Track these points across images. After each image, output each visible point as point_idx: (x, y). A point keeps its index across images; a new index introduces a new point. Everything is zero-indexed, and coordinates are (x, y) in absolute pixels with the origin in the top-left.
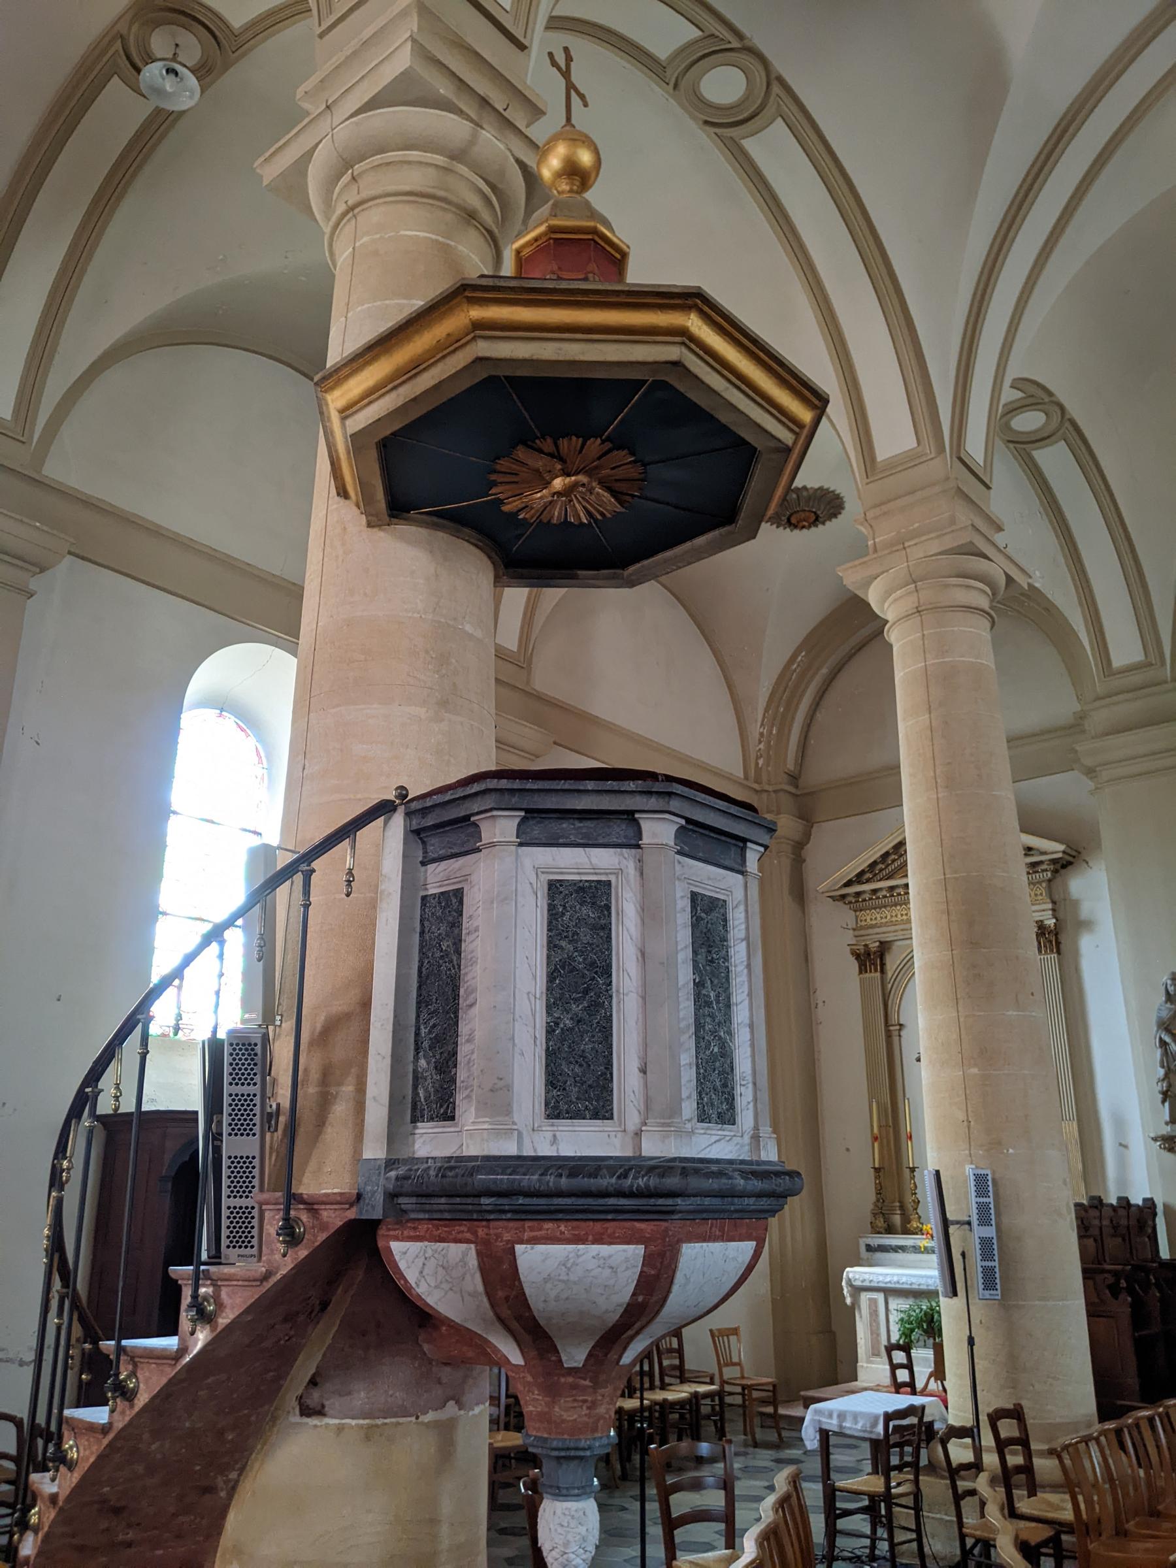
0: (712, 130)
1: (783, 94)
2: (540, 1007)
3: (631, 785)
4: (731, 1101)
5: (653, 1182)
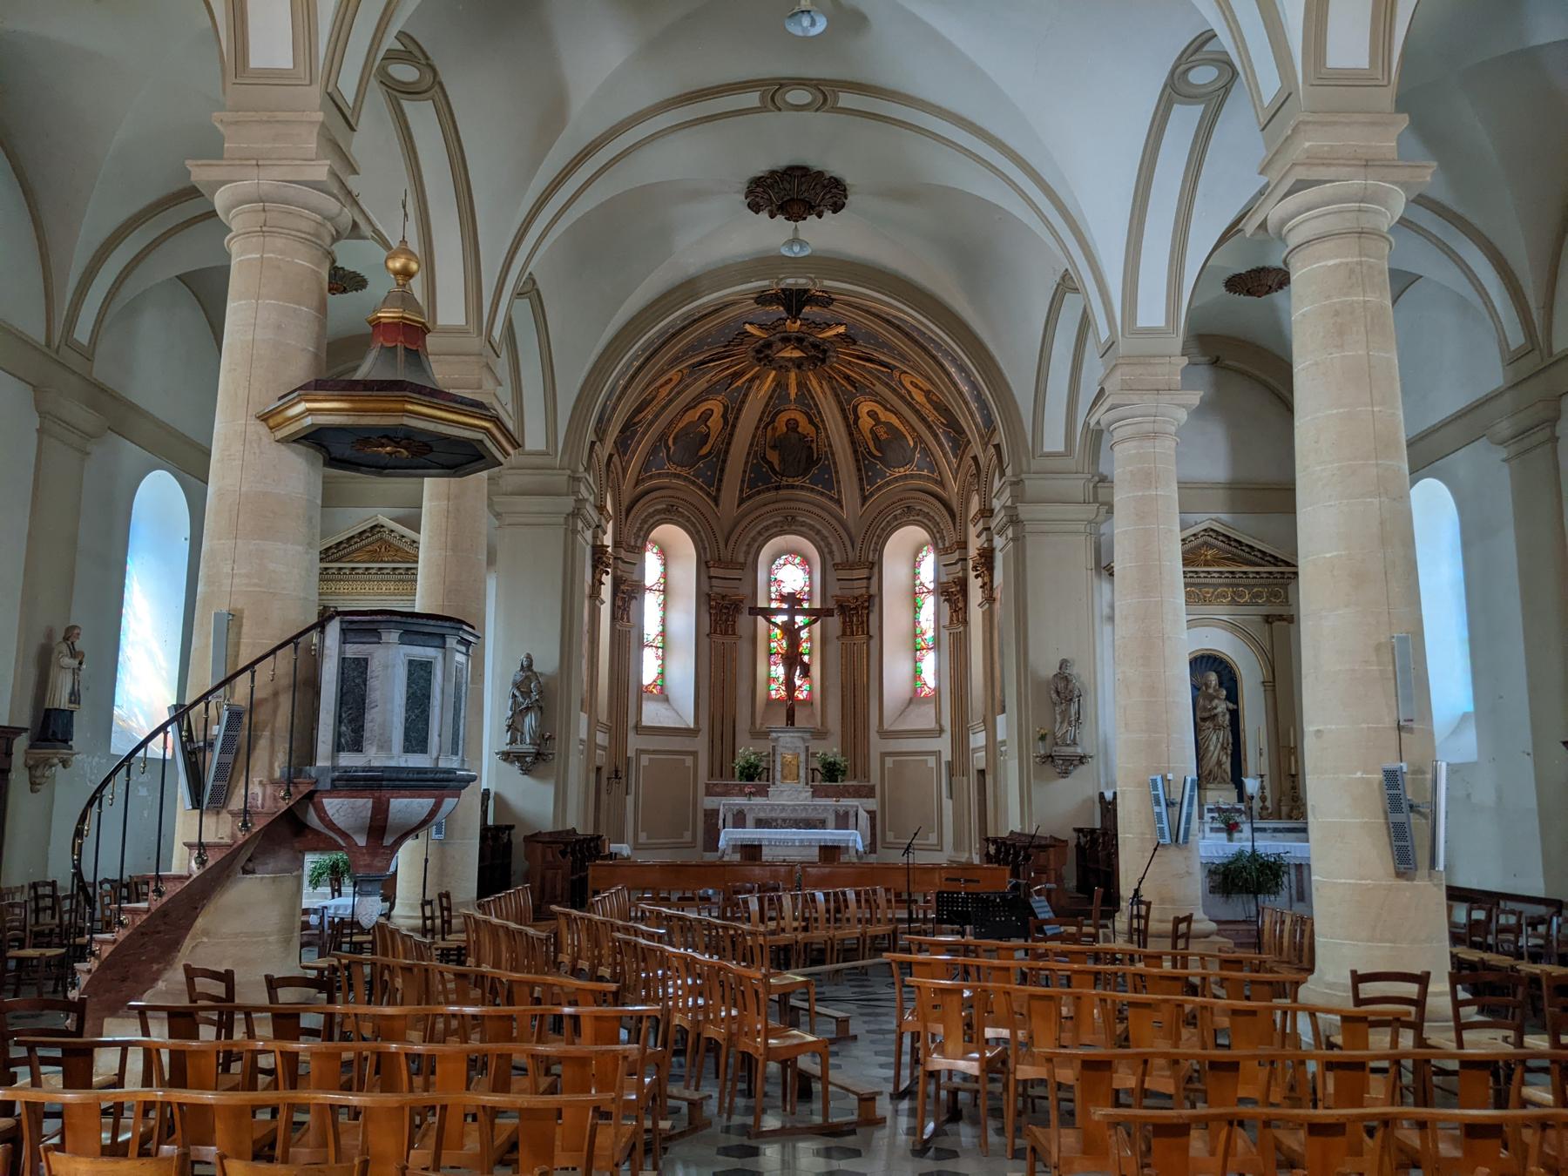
0: (384, 88)
1: (439, 91)
2: (403, 710)
3: (447, 624)
4: (425, 740)
5: (445, 776)
